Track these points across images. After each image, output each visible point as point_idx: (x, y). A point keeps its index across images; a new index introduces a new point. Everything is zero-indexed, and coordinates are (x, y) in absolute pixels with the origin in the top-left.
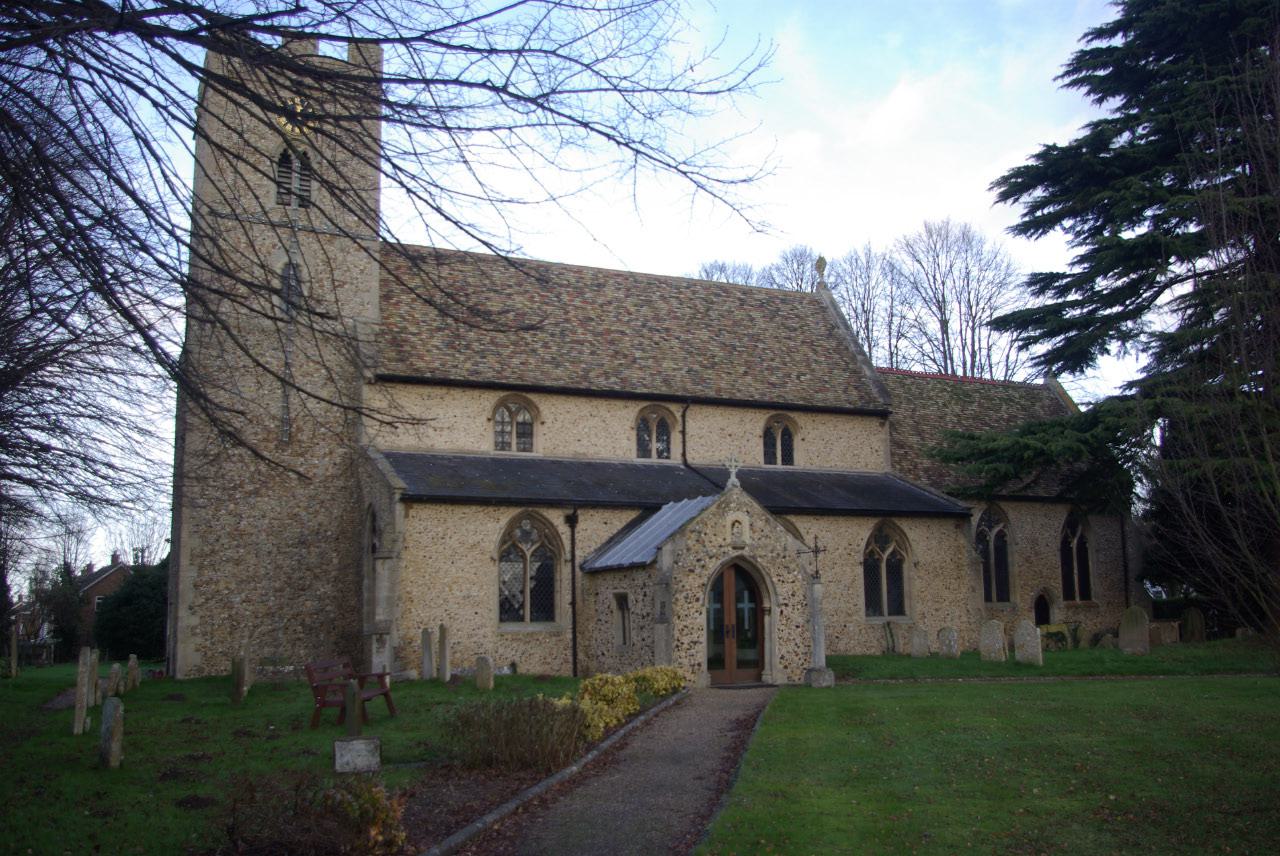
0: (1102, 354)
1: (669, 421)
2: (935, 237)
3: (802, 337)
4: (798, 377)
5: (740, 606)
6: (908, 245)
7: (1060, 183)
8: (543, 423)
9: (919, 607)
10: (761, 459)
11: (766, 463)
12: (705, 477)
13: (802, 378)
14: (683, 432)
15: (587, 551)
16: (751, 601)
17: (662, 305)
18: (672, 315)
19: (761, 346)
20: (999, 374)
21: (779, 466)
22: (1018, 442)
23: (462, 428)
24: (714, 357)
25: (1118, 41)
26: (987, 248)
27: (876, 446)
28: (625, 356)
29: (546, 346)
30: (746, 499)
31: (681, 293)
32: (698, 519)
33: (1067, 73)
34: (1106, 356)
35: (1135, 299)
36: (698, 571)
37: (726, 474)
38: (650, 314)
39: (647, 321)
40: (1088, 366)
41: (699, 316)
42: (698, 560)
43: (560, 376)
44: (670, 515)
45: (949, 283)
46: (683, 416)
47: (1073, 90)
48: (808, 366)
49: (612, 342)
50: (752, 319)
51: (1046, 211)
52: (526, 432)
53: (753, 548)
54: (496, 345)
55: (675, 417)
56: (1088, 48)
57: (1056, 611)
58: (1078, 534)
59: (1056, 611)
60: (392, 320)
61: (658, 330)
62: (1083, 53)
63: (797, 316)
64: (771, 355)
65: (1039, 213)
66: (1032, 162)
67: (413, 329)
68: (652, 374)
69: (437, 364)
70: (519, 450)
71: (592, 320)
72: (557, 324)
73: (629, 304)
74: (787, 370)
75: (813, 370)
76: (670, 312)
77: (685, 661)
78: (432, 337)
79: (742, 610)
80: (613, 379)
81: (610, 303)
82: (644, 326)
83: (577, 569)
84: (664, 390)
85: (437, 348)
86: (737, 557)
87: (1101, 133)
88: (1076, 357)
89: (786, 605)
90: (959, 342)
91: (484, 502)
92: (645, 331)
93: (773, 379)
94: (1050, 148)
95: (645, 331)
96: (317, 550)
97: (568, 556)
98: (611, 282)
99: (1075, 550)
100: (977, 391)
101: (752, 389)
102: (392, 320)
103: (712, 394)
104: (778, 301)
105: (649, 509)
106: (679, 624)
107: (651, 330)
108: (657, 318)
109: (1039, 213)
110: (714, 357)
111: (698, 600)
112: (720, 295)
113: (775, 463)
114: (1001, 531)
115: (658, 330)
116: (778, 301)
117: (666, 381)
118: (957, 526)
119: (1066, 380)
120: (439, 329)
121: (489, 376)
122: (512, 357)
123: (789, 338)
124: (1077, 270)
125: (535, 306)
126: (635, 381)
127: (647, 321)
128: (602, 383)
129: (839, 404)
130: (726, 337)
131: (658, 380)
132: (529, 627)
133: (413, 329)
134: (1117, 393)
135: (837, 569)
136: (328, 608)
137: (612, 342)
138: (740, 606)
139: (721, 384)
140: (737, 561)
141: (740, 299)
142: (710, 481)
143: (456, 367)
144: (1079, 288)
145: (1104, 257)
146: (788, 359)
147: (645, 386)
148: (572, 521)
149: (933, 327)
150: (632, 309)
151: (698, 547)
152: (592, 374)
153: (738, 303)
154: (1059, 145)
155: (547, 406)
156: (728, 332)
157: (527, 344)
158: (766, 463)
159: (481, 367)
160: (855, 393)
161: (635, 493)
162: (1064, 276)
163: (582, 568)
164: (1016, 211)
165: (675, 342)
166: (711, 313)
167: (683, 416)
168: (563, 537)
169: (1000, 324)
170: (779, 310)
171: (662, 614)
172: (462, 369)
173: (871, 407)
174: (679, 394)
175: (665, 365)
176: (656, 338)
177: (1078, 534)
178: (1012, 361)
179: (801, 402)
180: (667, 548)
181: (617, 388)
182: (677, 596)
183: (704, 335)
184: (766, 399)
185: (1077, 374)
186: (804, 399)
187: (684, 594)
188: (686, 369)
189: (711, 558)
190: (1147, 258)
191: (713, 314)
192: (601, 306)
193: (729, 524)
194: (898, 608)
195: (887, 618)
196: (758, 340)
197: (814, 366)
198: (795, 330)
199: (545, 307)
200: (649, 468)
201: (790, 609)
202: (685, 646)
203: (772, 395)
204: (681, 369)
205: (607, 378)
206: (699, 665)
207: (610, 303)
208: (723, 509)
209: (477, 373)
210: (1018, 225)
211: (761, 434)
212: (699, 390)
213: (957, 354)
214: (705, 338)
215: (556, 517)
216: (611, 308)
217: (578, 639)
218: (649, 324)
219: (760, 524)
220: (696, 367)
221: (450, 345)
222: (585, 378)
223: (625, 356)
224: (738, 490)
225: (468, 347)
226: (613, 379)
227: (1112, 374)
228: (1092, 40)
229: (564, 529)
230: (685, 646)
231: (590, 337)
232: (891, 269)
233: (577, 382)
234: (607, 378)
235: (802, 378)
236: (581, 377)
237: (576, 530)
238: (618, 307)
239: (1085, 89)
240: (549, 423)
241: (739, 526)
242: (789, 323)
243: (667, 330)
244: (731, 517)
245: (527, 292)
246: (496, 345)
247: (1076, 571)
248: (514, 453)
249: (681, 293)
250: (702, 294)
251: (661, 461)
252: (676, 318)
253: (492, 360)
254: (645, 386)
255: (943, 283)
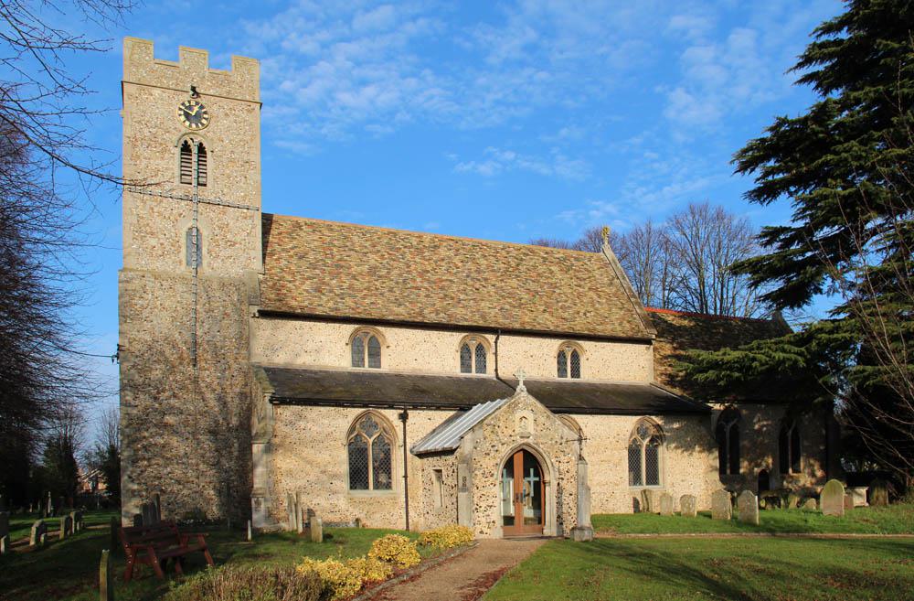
0: (816, 293)
1: (485, 346)
2: (697, 217)
3: (589, 285)
4: (585, 314)
5: (537, 479)
6: (678, 222)
7: (787, 154)
8: (388, 347)
9: (669, 480)
10: (556, 375)
11: (559, 376)
12: (509, 386)
13: (588, 315)
14: (496, 354)
15: (416, 439)
16: (535, 476)
17: (483, 261)
18: (490, 268)
19: (558, 291)
20: (739, 314)
21: (569, 379)
22: (746, 355)
23: (327, 349)
24: (520, 299)
25: (844, 35)
26: (735, 223)
27: (642, 364)
28: (452, 298)
29: (391, 290)
30: (532, 400)
31: (498, 252)
32: (493, 415)
33: (800, 65)
34: (819, 295)
35: (843, 248)
36: (492, 454)
37: (517, 382)
38: (474, 268)
39: (470, 273)
40: (805, 302)
41: (511, 269)
42: (493, 446)
43: (401, 313)
44: (478, 412)
45: (706, 249)
46: (496, 343)
47: (805, 85)
48: (593, 306)
49: (442, 288)
50: (552, 272)
51: (777, 177)
52: (375, 355)
53: (536, 437)
54: (353, 289)
55: (489, 343)
56: (818, 42)
57: (774, 480)
58: (794, 425)
59: (774, 480)
60: (273, 271)
61: (479, 280)
62: (814, 44)
63: (586, 270)
64: (565, 298)
65: (770, 178)
66: (768, 135)
67: (289, 278)
68: (472, 312)
69: (306, 303)
70: (370, 366)
71: (428, 272)
72: (400, 275)
73: (456, 260)
74: (576, 308)
75: (597, 309)
76: (488, 266)
77: (483, 520)
78: (303, 283)
79: (535, 476)
80: (442, 315)
81: (443, 260)
82: (468, 276)
83: (408, 452)
84: (481, 323)
85: (307, 291)
86: (523, 444)
87: (821, 113)
88: (796, 296)
89: (562, 479)
90: (712, 292)
91: (338, 403)
92: (469, 280)
93: (566, 315)
94: (783, 122)
95: (469, 280)
96: (223, 437)
97: (401, 443)
98: (445, 244)
99: (790, 438)
100: (722, 325)
101: (549, 322)
102: (273, 271)
103: (517, 326)
104: (572, 259)
105: (464, 408)
106: (477, 493)
107: (473, 279)
108: (478, 271)
109: (770, 178)
110: (520, 299)
111: (492, 475)
112: (528, 255)
113: (566, 377)
114: (735, 425)
115: (479, 280)
116: (572, 259)
117: (483, 317)
118: (700, 421)
119: (786, 312)
120: (309, 278)
121: (349, 313)
122: (364, 299)
123: (580, 286)
124: (800, 224)
125: (385, 262)
126: (458, 316)
127: (470, 273)
128: (432, 318)
129: (615, 334)
130: (532, 286)
131: (477, 317)
132: (371, 492)
133: (289, 278)
134: (826, 317)
135: (608, 452)
136: (233, 478)
137: (442, 288)
138: (537, 479)
139: (526, 319)
140: (525, 447)
141: (543, 258)
142: (504, 389)
143: (321, 305)
144: (801, 240)
145: (818, 212)
146: (578, 301)
147: (466, 320)
148: (404, 417)
149: (694, 282)
150: (460, 264)
151: (493, 436)
152: (426, 311)
153: (541, 260)
154: (789, 118)
155: (390, 334)
156: (534, 281)
157: (377, 289)
158: (559, 376)
159: (340, 305)
160: (628, 325)
161: (454, 397)
162: (789, 229)
163: (411, 451)
164: (752, 180)
165: (492, 290)
166: (520, 267)
167: (496, 343)
168: (397, 429)
169: (737, 269)
170: (573, 265)
171: (464, 485)
172: (325, 305)
173: (640, 335)
174: (493, 326)
175: (483, 304)
176: (477, 286)
177: (794, 425)
178: (747, 301)
179: (586, 332)
180: (468, 437)
181: (444, 321)
182: (476, 472)
183: (514, 282)
184: (559, 329)
185: (796, 309)
186: (589, 330)
187: (482, 471)
188: (498, 308)
189: (503, 444)
190: (853, 208)
191: (522, 268)
192: (436, 262)
193: (517, 420)
194: (653, 478)
195: (645, 487)
196: (556, 287)
197: (597, 305)
198: (585, 279)
199: (392, 263)
200: (469, 380)
201: (565, 481)
202: (483, 508)
203: (564, 327)
204: (495, 308)
205: (437, 314)
206: (494, 522)
207: (443, 260)
208: (513, 408)
209: (337, 309)
210: (754, 191)
211: (556, 356)
212: (506, 323)
213: (710, 301)
214: (516, 286)
215: (392, 415)
216: (443, 264)
217: (409, 503)
218: (472, 275)
219: (542, 419)
220: (507, 307)
221: (318, 290)
222: (421, 314)
223: (452, 298)
224: (525, 394)
225: (331, 291)
226: (442, 315)
227: (821, 308)
228: (820, 35)
229: (398, 424)
230: (483, 508)
231: (426, 285)
232: (666, 244)
233: (414, 317)
234: (437, 314)
235: (588, 315)
236: (417, 313)
237: (407, 424)
238: (449, 263)
239: (813, 84)
240: (392, 347)
241: (526, 422)
242: (580, 275)
243: (486, 279)
244: (519, 414)
245: (379, 251)
246: (353, 289)
247: (790, 453)
248: (366, 368)
249: (498, 252)
250: (514, 253)
251: (478, 375)
252: (493, 271)
253: (349, 301)
254: (466, 320)
255: (702, 250)
